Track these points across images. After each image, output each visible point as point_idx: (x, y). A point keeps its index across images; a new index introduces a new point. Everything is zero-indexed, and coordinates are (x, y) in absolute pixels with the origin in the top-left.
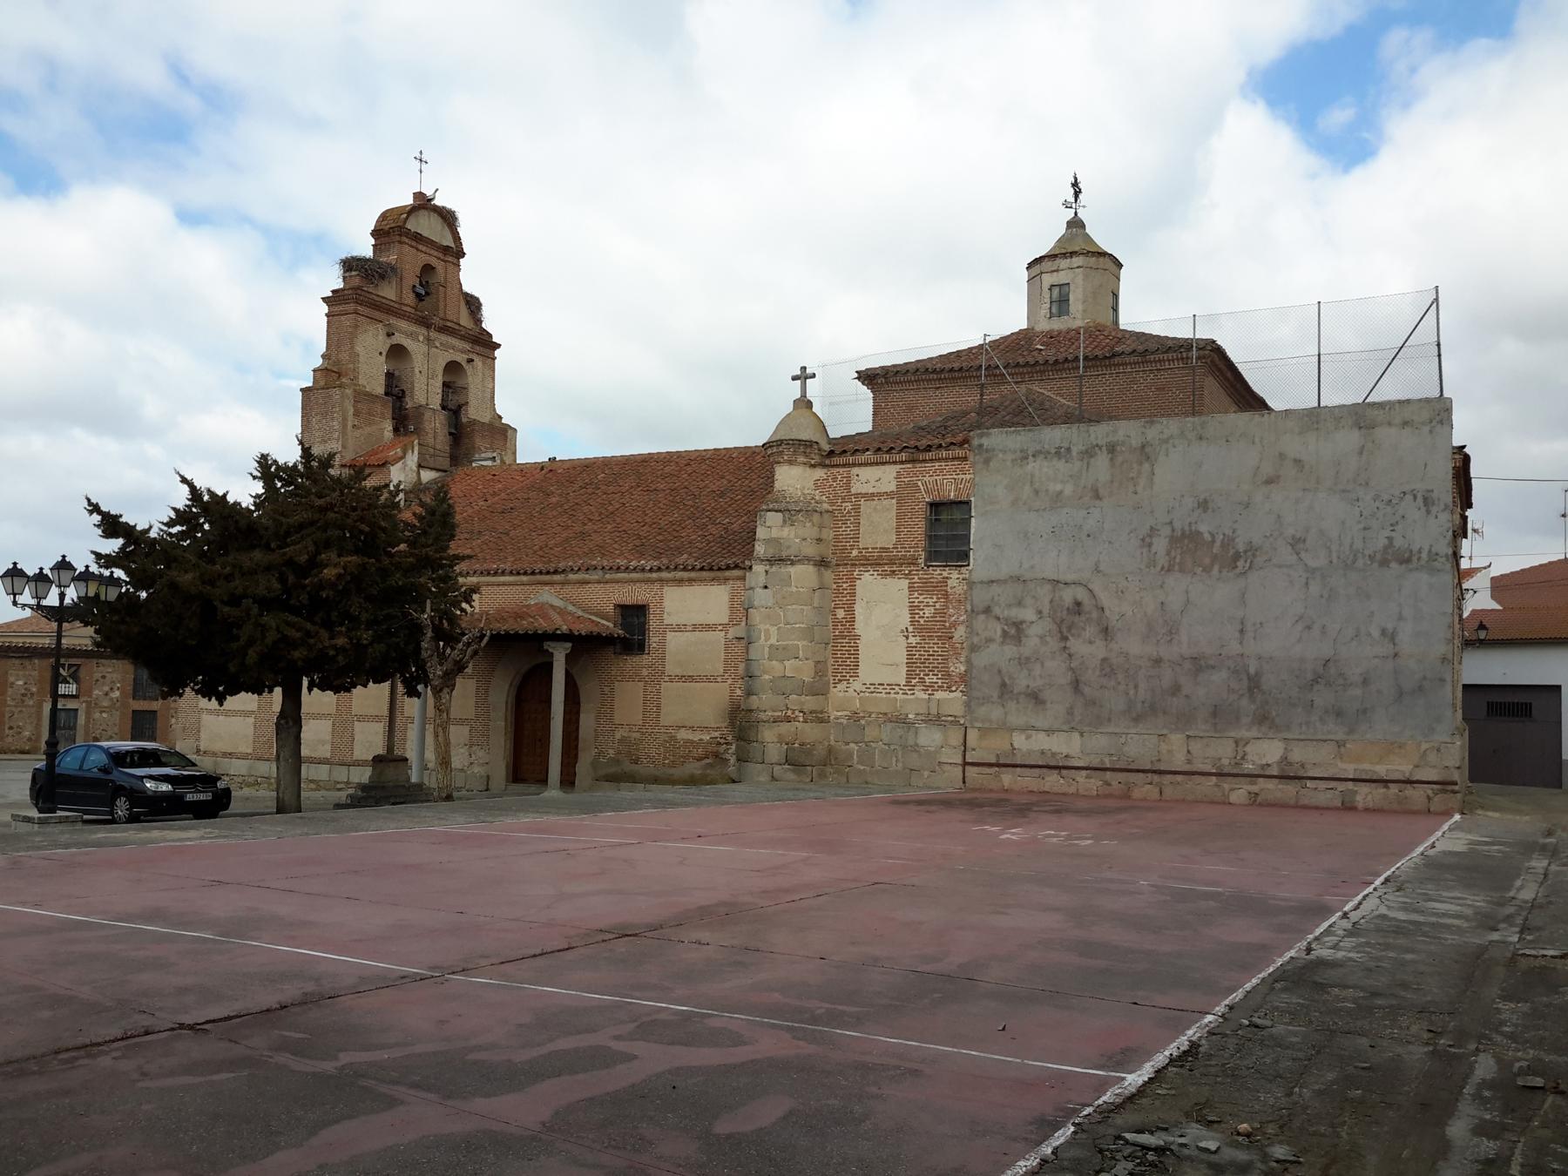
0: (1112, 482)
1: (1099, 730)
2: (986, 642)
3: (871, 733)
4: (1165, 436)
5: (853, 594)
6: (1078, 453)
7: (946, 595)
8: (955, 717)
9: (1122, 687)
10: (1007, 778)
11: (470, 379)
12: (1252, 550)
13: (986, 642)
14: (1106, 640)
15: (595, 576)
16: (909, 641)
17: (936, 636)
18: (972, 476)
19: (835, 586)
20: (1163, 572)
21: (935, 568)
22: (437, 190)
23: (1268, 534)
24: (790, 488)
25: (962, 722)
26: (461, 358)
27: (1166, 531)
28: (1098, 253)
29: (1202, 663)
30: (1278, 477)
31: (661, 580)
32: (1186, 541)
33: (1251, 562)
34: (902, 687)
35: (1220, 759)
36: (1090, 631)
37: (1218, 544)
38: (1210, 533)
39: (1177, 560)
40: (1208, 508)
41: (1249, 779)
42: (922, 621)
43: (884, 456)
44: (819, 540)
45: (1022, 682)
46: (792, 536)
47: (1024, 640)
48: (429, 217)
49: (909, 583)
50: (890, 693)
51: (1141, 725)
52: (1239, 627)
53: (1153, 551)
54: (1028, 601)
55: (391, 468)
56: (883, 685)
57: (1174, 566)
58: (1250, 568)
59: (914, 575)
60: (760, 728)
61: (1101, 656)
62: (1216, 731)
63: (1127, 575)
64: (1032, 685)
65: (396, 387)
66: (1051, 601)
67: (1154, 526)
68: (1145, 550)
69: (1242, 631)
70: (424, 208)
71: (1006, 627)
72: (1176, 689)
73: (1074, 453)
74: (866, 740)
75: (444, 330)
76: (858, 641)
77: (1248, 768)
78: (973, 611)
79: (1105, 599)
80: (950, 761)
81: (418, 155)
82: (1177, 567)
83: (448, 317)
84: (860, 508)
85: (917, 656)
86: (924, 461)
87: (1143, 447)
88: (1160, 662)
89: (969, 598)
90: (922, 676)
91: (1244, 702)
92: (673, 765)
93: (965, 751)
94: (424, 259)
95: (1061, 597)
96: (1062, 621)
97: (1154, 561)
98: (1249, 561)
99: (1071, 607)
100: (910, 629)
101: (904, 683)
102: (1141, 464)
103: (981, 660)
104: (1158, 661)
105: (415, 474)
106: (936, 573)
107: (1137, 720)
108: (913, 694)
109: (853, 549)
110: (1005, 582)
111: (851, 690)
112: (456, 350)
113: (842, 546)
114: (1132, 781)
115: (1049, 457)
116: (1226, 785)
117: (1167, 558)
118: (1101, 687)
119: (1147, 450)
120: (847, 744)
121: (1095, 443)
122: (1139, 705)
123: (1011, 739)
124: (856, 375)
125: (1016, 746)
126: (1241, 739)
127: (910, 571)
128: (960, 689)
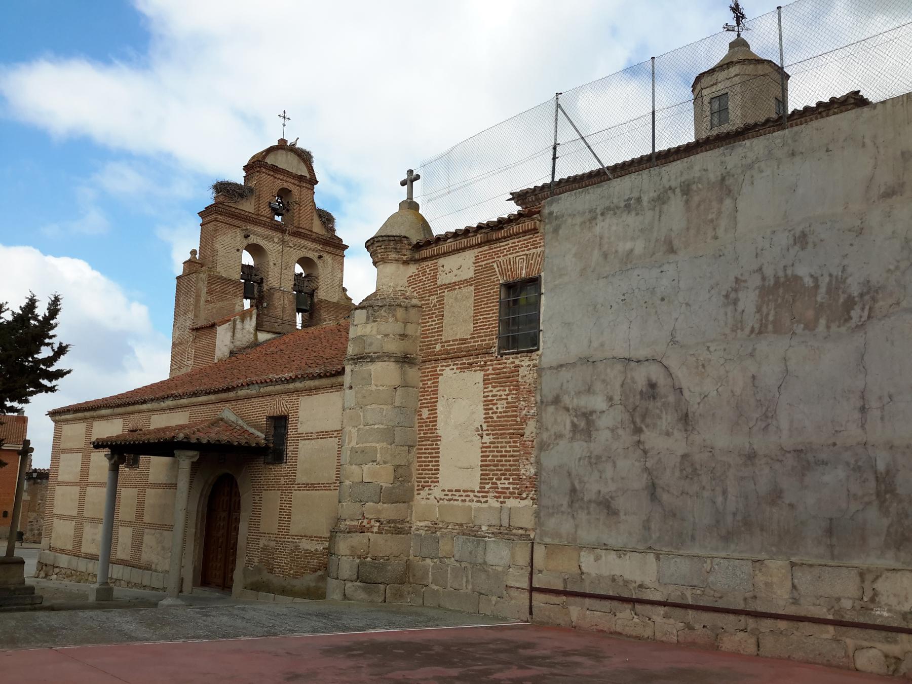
0: (688, 229)
1: (681, 552)
2: (556, 439)
3: (445, 547)
4: (749, 161)
5: (436, 392)
6: (649, 202)
7: (517, 388)
8: (526, 530)
9: (706, 494)
10: (576, 611)
11: (321, 271)
12: (871, 292)
13: (556, 439)
14: (686, 430)
15: (252, 391)
16: (484, 441)
17: (509, 434)
18: (542, 249)
19: (421, 384)
20: (753, 336)
21: (507, 356)
22: (298, 139)
23: (892, 267)
24: (384, 287)
25: (532, 537)
26: (313, 255)
27: (756, 280)
28: (755, 60)
29: (810, 457)
30: (902, 185)
31: (296, 391)
32: (781, 291)
33: (870, 309)
34: (476, 494)
35: (838, 599)
36: (667, 420)
37: (823, 290)
38: (812, 276)
39: (771, 318)
40: (807, 243)
41: (884, 634)
42: (495, 416)
43: (463, 240)
44: (403, 336)
45: (593, 487)
46: (374, 332)
47: (594, 434)
48: (287, 156)
49: (484, 375)
50: (465, 501)
51: (733, 546)
52: (859, 404)
53: (740, 309)
54: (598, 386)
55: (218, 328)
56: (452, 491)
57: (766, 327)
58: (869, 317)
59: (489, 365)
60: (337, 538)
61: (680, 452)
62: (833, 557)
63: (709, 344)
64: (604, 490)
65: (256, 275)
66: (622, 386)
67: (739, 277)
68: (730, 309)
69: (863, 409)
70: (282, 149)
71: (575, 420)
72: (775, 496)
73: (645, 203)
74: (440, 555)
75: (297, 234)
76: (439, 443)
77: (881, 616)
78: (542, 402)
79: (683, 376)
80: (517, 585)
81: (282, 114)
82: (770, 327)
83: (301, 226)
84: (444, 300)
85: (490, 458)
86: (498, 240)
87: (723, 179)
88: (755, 456)
89: (539, 387)
90: (494, 480)
91: (873, 514)
92: (295, 576)
93: (531, 574)
94: (279, 184)
95: (633, 378)
96: (634, 409)
97: (741, 322)
98: (867, 307)
99: (644, 390)
100: (485, 427)
101: (479, 489)
102: (721, 201)
103: (550, 460)
104: (751, 457)
105: (252, 336)
106: (509, 361)
107: (727, 537)
108: (486, 502)
109: (436, 344)
110: (574, 364)
111: (432, 497)
112: (311, 250)
113: (428, 341)
114: (720, 625)
115: (618, 212)
116: (851, 639)
117: (758, 316)
118: (683, 493)
119: (727, 183)
120: (424, 559)
121: (667, 186)
122: (729, 519)
123: (579, 560)
124: (511, 197)
125: (584, 569)
126: (869, 570)
127: (486, 362)
128: (531, 496)
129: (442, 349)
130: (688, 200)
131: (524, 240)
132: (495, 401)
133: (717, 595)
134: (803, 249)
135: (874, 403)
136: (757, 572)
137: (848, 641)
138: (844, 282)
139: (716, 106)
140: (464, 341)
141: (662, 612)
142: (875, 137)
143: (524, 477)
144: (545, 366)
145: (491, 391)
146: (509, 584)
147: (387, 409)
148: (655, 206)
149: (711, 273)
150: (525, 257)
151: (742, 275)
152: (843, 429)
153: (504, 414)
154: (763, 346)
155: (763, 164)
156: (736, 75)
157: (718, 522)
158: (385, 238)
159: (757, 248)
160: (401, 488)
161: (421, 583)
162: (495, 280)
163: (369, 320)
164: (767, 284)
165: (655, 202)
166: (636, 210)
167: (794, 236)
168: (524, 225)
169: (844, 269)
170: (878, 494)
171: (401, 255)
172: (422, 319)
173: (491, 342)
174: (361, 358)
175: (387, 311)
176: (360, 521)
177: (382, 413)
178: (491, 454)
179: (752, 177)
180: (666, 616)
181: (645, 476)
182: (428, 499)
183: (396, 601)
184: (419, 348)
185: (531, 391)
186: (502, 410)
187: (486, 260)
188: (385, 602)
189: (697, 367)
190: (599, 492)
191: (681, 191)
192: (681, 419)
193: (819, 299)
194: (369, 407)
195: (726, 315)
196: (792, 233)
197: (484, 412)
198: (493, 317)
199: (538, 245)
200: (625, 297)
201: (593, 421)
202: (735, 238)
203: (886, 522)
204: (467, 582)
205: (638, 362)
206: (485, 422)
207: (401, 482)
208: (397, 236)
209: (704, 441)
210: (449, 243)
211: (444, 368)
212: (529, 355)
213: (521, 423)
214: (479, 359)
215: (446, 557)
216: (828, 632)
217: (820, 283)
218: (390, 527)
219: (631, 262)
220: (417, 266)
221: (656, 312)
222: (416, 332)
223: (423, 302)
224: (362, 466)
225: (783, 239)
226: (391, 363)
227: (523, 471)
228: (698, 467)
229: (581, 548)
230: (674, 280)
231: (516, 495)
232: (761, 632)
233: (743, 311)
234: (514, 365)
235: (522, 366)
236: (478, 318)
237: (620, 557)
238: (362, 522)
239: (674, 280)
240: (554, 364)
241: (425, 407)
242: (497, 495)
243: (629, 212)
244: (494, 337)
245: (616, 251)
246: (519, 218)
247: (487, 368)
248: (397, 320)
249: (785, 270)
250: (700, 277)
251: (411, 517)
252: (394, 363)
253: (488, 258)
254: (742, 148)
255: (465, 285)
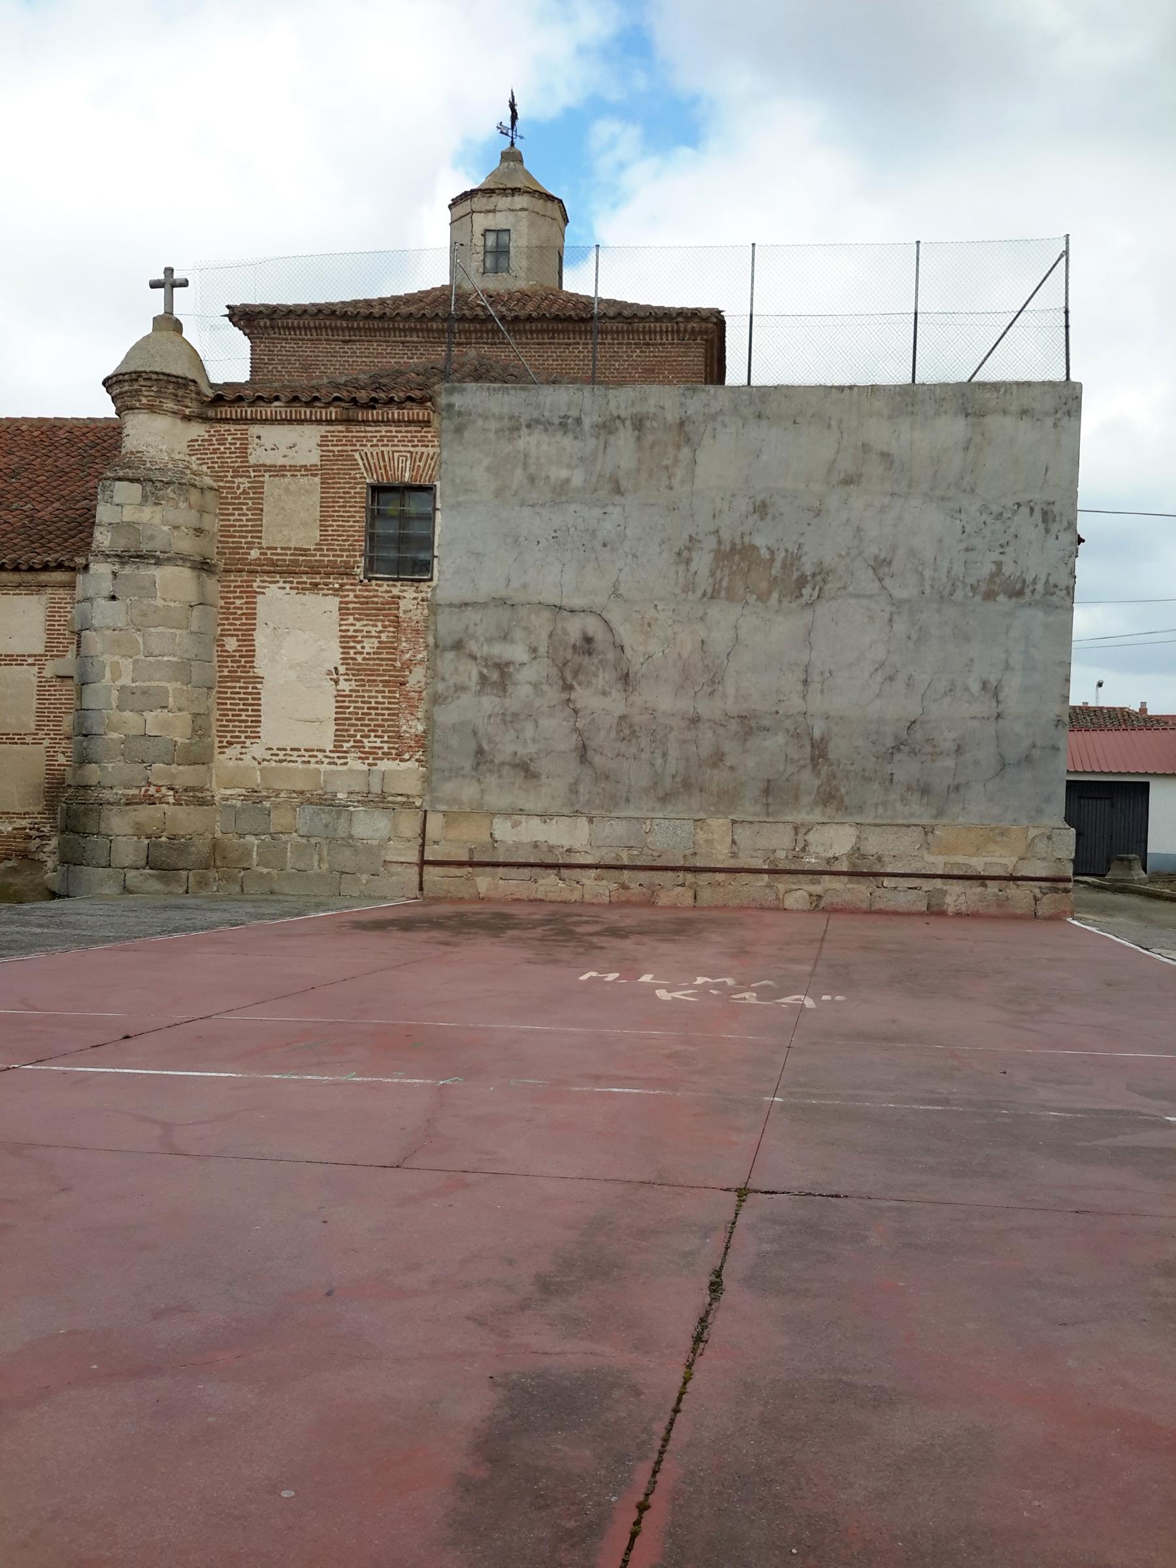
0: (639, 470)
1: (613, 815)
2: (456, 691)
3: (279, 819)
4: (713, 411)
5: (252, 616)
6: (592, 427)
7: (397, 622)
8: (408, 796)
9: (645, 756)
10: (484, 882)
12: (822, 573)
13: (456, 691)
16: (338, 688)
20: (705, 599)
21: (380, 582)
29: (753, 723)
30: (860, 476)
32: (737, 557)
34: (328, 754)
36: (604, 678)
37: (778, 564)
38: (768, 548)
39: (725, 584)
41: (810, 877)
42: (359, 658)
44: (199, 531)
47: (510, 689)
49: (341, 602)
50: (309, 762)
51: (670, 808)
52: (802, 677)
53: (692, 570)
54: (518, 634)
57: (719, 592)
58: (818, 597)
61: (618, 713)
62: (768, 814)
63: (656, 602)
64: (522, 751)
66: (550, 636)
67: (694, 535)
68: (682, 568)
69: (805, 682)
72: (717, 758)
74: (272, 831)
76: (258, 686)
78: (436, 646)
79: (625, 633)
85: (351, 710)
86: (365, 422)
87: (682, 424)
88: (698, 721)
89: (432, 628)
90: (358, 738)
91: (806, 776)
93: (423, 845)
96: (565, 664)
98: (817, 588)
99: (578, 644)
100: (342, 670)
101: (332, 749)
102: (678, 447)
103: (447, 716)
104: (695, 721)
107: (664, 799)
108: (346, 764)
110: (485, 605)
114: (658, 882)
115: (551, 429)
117: (711, 580)
120: (241, 836)
122: (668, 781)
125: (497, 836)
127: (342, 585)
129: (262, 557)
130: (640, 437)
131: (407, 432)
132: (359, 639)
133: (655, 854)
134: (762, 519)
135: (815, 677)
136: (698, 830)
137: (780, 886)
138: (799, 559)
139: (491, 240)
140: (304, 551)
141: (593, 875)
142: (841, 421)
143: (407, 735)
144: (441, 603)
145: (354, 625)
146: (388, 858)
147: (181, 635)
148: (600, 434)
149: (663, 525)
150: (409, 455)
151: (697, 534)
152: (785, 698)
153: (376, 656)
154: (715, 611)
155: (727, 419)
156: (522, 209)
157: (656, 783)
158: (161, 377)
159: (715, 509)
160: (200, 744)
161: (238, 866)
162: (358, 476)
163: (147, 501)
164: (722, 548)
165: (600, 429)
166: (574, 433)
167: (754, 503)
168: (411, 412)
169: (800, 546)
170: (812, 759)
171: (182, 406)
172: (220, 509)
173: (352, 560)
174: (138, 557)
175: (177, 492)
176: (143, 789)
177: (174, 640)
178: (353, 705)
179: (715, 429)
180: (598, 878)
181: (575, 736)
182: (242, 760)
183: (201, 891)
184: (216, 550)
185: (419, 630)
186: (371, 651)
187: (341, 445)
188: (187, 892)
189: (642, 625)
190: (516, 753)
191: (633, 424)
192: (621, 679)
193: (773, 572)
194: (153, 630)
195: (678, 574)
196: (753, 500)
197: (342, 650)
198: (355, 526)
199: (430, 444)
200: (557, 535)
201: (510, 675)
202: (692, 492)
203: (817, 782)
204: (319, 861)
205: (572, 611)
206: (342, 664)
207: (200, 736)
208: (182, 378)
209: (645, 702)
210: (276, 407)
211: (267, 584)
212: (416, 584)
213: (402, 669)
214: (331, 580)
215: (282, 833)
216: (762, 880)
217: (776, 556)
218: (189, 797)
219: (566, 494)
220: (207, 426)
221: (596, 559)
222: (213, 527)
223: (221, 484)
224: (144, 713)
225: (743, 505)
226: (186, 569)
227: (404, 728)
228: (637, 729)
229: (494, 815)
230: (619, 525)
231: (394, 756)
232: (698, 886)
233: (696, 573)
234: (390, 595)
235: (404, 598)
236: (328, 523)
237: (545, 822)
238: (147, 791)
239: (619, 525)
240: (456, 601)
241: (232, 635)
242: (363, 755)
243: (565, 433)
244: (358, 554)
245: (547, 477)
246: (406, 401)
247: (346, 593)
248: (190, 507)
249: (743, 538)
250: (651, 528)
251: (211, 783)
252: (189, 570)
253: (344, 442)
254: (705, 394)
255: (303, 473)
